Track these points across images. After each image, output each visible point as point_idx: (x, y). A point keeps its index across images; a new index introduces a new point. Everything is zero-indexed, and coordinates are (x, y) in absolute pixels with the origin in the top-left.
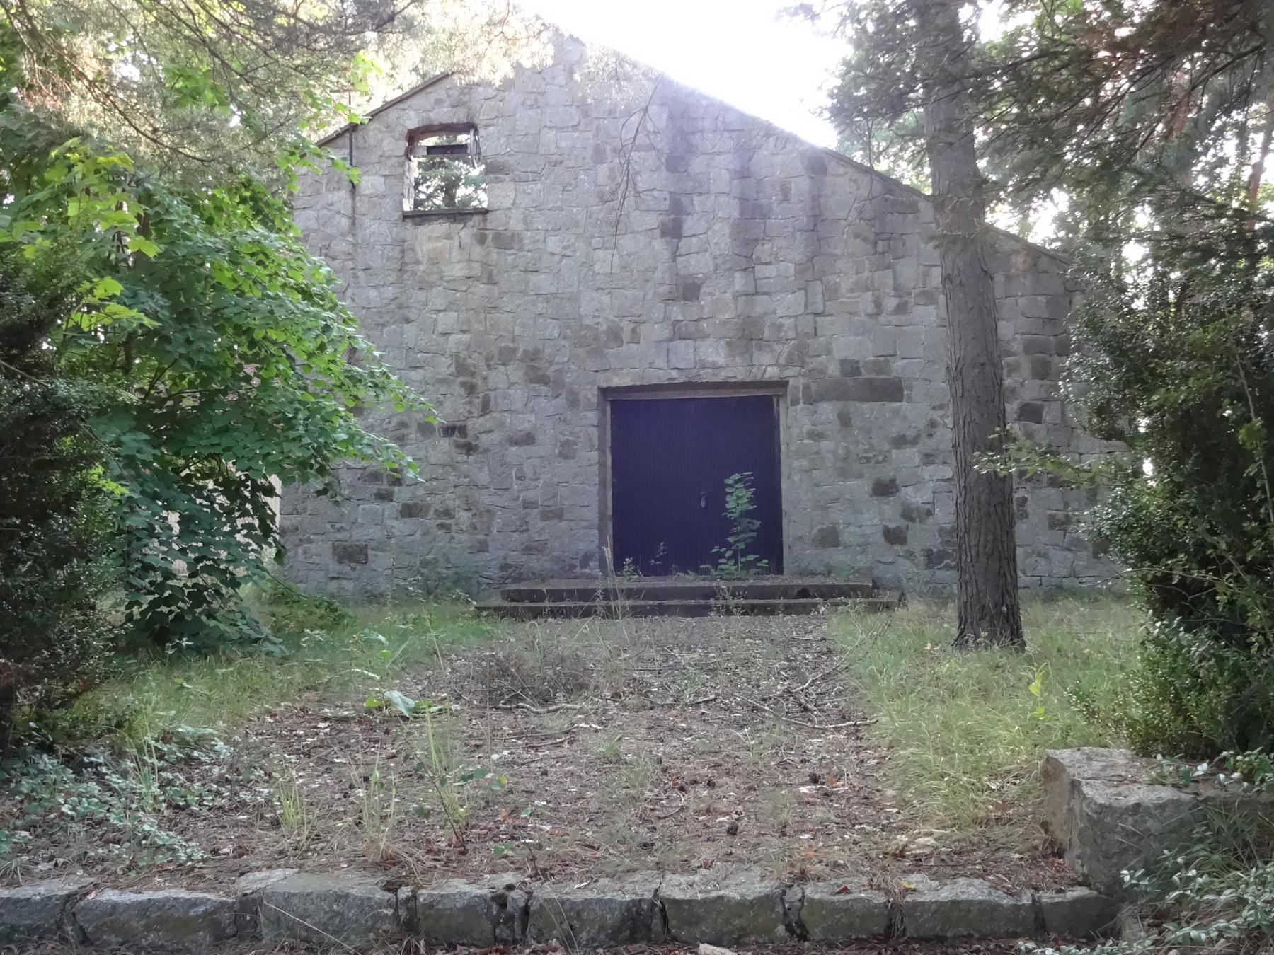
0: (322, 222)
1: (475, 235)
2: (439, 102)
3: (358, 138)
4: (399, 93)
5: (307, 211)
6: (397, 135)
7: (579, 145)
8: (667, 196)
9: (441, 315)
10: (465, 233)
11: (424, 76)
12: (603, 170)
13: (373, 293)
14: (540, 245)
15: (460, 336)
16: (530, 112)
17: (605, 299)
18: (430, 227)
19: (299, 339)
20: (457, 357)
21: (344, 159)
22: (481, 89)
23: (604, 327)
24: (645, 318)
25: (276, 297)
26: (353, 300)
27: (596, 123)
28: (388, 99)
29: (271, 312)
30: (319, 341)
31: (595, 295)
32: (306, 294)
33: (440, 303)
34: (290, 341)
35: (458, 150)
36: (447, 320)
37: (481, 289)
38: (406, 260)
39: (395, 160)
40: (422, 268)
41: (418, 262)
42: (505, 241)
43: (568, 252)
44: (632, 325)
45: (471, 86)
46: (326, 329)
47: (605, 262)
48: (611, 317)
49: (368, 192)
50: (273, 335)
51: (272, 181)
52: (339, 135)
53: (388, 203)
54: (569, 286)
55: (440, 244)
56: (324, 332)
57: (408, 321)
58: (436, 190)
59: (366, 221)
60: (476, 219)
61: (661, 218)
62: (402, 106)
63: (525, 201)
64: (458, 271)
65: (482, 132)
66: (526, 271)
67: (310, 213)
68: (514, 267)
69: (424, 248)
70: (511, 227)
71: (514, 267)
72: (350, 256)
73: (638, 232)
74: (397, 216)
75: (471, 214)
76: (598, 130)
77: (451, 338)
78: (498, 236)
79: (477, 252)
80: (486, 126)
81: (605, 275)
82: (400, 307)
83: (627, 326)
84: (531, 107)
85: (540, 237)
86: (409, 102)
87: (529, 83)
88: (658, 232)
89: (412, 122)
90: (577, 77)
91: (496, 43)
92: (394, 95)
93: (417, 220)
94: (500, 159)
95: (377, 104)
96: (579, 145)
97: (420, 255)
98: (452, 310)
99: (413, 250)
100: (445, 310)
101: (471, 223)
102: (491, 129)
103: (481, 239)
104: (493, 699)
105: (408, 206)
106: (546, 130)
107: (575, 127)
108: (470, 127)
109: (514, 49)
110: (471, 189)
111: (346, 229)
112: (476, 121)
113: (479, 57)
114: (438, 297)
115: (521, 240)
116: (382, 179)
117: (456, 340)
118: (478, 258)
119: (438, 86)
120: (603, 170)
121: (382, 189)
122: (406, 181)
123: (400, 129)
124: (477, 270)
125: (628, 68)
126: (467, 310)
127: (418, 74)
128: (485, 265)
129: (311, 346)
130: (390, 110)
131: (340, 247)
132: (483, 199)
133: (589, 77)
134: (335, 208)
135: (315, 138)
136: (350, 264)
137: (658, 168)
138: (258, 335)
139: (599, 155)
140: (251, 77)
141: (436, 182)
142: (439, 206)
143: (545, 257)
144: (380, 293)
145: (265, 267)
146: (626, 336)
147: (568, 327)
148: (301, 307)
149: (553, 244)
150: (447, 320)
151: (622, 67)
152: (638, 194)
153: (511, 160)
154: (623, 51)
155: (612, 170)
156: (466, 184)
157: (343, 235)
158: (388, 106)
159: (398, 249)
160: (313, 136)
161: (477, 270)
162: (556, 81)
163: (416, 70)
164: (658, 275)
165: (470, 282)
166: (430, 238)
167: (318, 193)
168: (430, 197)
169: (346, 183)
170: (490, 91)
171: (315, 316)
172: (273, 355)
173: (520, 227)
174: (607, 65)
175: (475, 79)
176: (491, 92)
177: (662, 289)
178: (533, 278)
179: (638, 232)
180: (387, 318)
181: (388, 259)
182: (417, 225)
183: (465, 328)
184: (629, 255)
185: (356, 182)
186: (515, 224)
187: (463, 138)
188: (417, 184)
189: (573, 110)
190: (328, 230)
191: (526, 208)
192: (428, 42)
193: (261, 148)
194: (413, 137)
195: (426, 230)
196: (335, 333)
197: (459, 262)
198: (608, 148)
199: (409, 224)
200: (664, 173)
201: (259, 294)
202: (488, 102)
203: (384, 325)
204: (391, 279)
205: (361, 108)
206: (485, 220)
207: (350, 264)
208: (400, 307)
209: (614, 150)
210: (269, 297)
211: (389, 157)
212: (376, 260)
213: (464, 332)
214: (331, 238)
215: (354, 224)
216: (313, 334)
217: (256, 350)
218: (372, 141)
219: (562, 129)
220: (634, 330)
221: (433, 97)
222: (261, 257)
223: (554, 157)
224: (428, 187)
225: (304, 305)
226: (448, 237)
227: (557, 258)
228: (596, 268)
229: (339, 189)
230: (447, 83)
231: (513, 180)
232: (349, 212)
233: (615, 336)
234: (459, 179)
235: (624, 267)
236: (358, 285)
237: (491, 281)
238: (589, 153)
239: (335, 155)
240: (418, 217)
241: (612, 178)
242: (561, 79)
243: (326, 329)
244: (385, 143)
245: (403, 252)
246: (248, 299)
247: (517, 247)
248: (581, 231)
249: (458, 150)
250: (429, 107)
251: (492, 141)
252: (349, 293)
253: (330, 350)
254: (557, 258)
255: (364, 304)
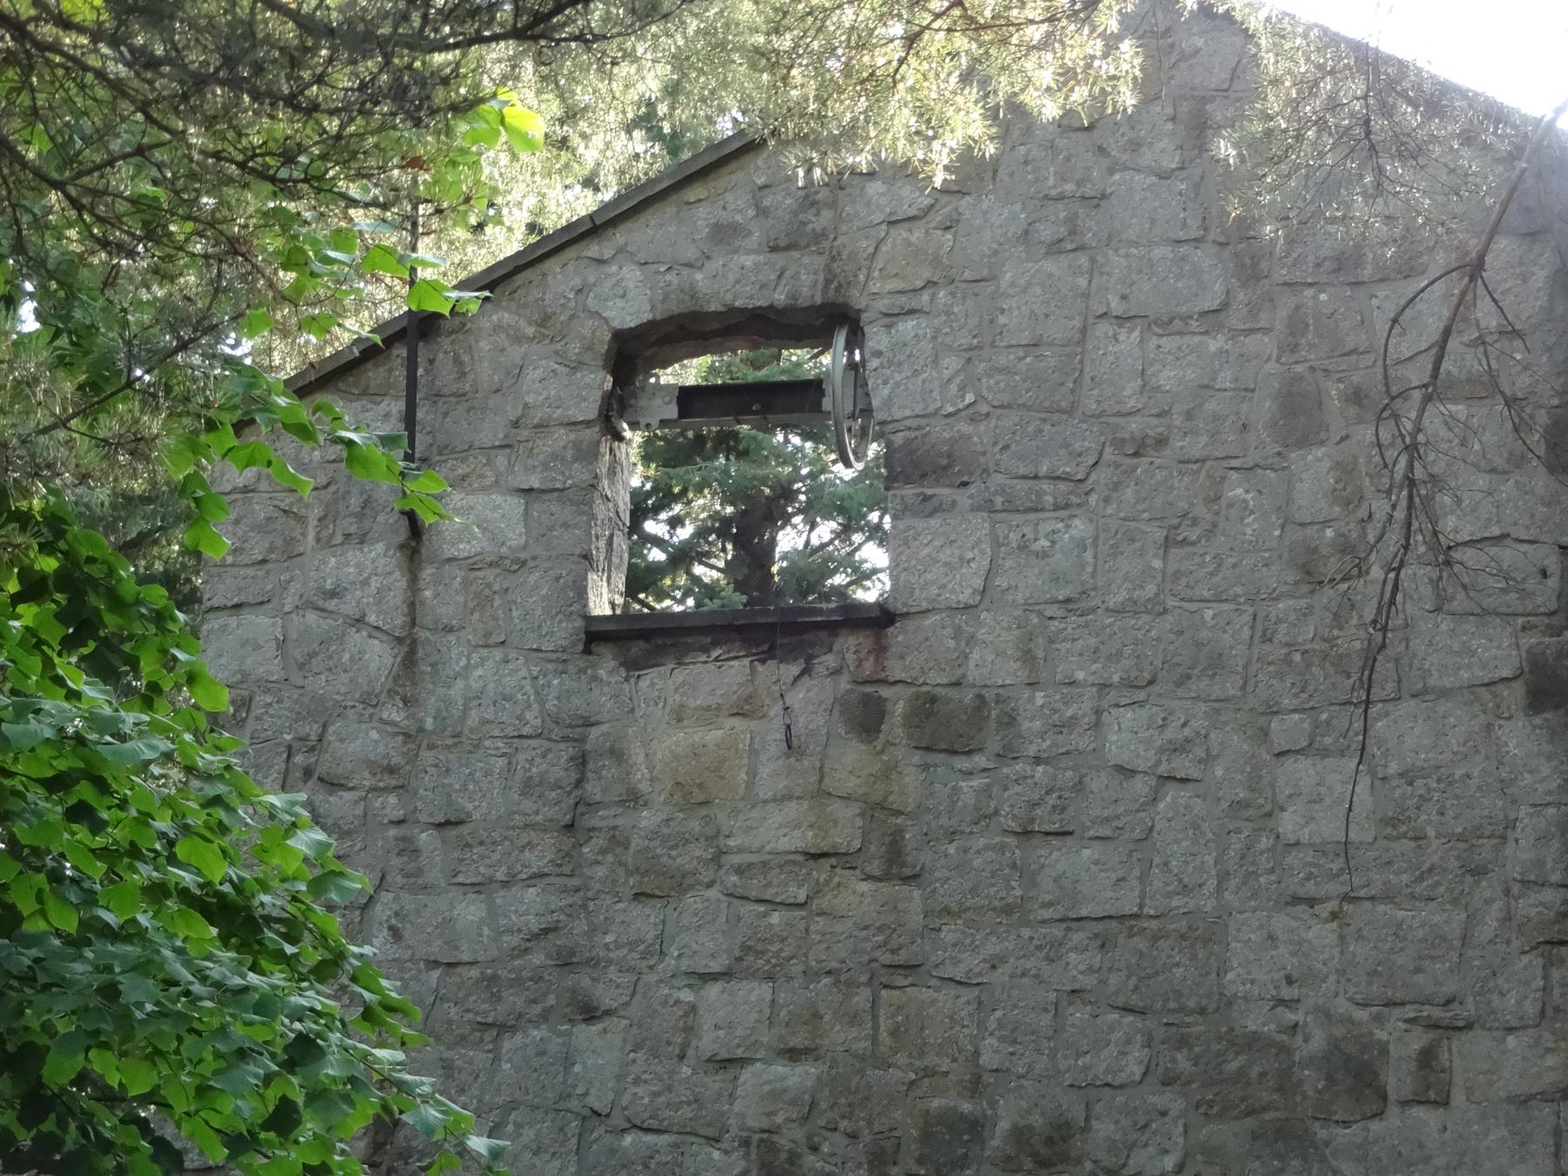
0: (298, 654)
1: (841, 702)
2: (724, 234)
3: (439, 362)
4: (584, 204)
5: (248, 617)
6: (575, 348)
7: (1225, 378)
8: (1553, 562)
9: (713, 991)
10: (810, 695)
11: (673, 144)
12: (1314, 470)
13: (470, 911)
14: (1084, 742)
15: (780, 1069)
16: (1050, 266)
17: (1321, 935)
18: (681, 675)
19: (203, 1091)
20: (769, 1147)
21: (388, 441)
22: (874, 188)
23: (1318, 1042)
24: (1470, 1008)
25: (129, 933)
26: (396, 934)
27: (1286, 305)
28: (551, 223)
29: (110, 992)
30: (273, 1095)
31: (1281, 922)
32: (232, 916)
33: (710, 949)
34: (168, 1093)
35: (798, 400)
36: (734, 1011)
37: (858, 896)
38: (593, 790)
39: (562, 437)
40: (647, 819)
41: (633, 799)
42: (950, 726)
43: (1183, 765)
44: (1418, 1040)
45: (840, 182)
46: (303, 1051)
47: (1320, 800)
48: (1342, 1006)
49: (464, 549)
50: (108, 1068)
51: (128, 502)
52: (368, 353)
53: (535, 590)
54: (1185, 889)
55: (714, 736)
56: (290, 1065)
57: (590, 1013)
58: (702, 533)
59: (456, 653)
60: (851, 644)
61: (1530, 640)
62: (593, 249)
63: (1025, 582)
64: (778, 830)
65: (876, 337)
66: (1026, 834)
67: (261, 624)
68: (984, 817)
69: (661, 752)
70: (973, 674)
71: (984, 817)
72: (393, 776)
73: (1444, 694)
74: (565, 632)
75: (832, 628)
76: (1297, 326)
77: (747, 1075)
78: (926, 708)
79: (851, 762)
80: (892, 317)
81: (1320, 850)
82: (566, 962)
83: (1401, 1041)
84: (1054, 248)
85: (1083, 708)
86: (620, 236)
87: (1050, 175)
88: (1515, 694)
89: (627, 296)
90: (1225, 149)
91: (935, 42)
92: (571, 204)
93: (637, 648)
94: (941, 432)
95: (506, 242)
96: (1225, 378)
97: (641, 775)
98: (751, 975)
99: (617, 755)
100: (726, 975)
101: (830, 660)
102: (908, 326)
103: (866, 718)
104: (1164, 1084)
105: (603, 599)
106: (1104, 328)
107: (1213, 318)
108: (831, 320)
109: (999, 56)
110: (825, 530)
111: (381, 681)
112: (858, 299)
113: (878, 85)
114: (703, 928)
115: (1009, 721)
116: (515, 505)
117: (769, 1083)
118: (851, 784)
119: (723, 180)
120: (1314, 470)
121: (515, 536)
122: (601, 510)
123: (586, 327)
124: (846, 829)
125: (1410, 117)
126: (810, 975)
127: (655, 134)
128: (877, 809)
129: (243, 1106)
130: (553, 264)
131: (359, 743)
132: (874, 571)
133: (1264, 150)
134: (348, 606)
135: (285, 362)
136: (392, 806)
137: (1517, 461)
138: (58, 1071)
139: (1298, 418)
140: (97, 193)
141: (706, 504)
142: (711, 591)
143: (1097, 783)
144: (493, 913)
145: (97, 826)
146: (1397, 1079)
147: (1183, 1042)
148: (215, 972)
149: (1128, 735)
150: (734, 1011)
151: (1387, 111)
152: (1444, 555)
153: (979, 435)
154: (1392, 42)
155: (1345, 469)
156: (812, 513)
157: (370, 701)
158: (549, 247)
159: (565, 752)
160: (270, 351)
161: (846, 829)
162: (1147, 157)
163: (646, 121)
164: (1520, 854)
165: (821, 872)
166: (679, 716)
167: (291, 554)
168: (682, 557)
169: (388, 521)
170: (907, 191)
171: (266, 1007)
172: (106, 1146)
173: (1009, 673)
174: (1333, 105)
175: (863, 161)
176: (909, 199)
177: (1530, 906)
178: (1057, 860)
179: (1444, 694)
180: (514, 1000)
181: (528, 786)
182: (633, 666)
183: (798, 1041)
184: (1408, 776)
185: (428, 519)
186: (991, 662)
187: (799, 360)
188: (641, 510)
189: (1204, 257)
190: (319, 684)
191: (1028, 607)
192: (693, 25)
193: (108, 426)
194: (630, 355)
195: (663, 683)
196: (331, 1070)
197: (787, 797)
198: (1334, 391)
199: (607, 665)
200: (1541, 481)
201: (70, 925)
202: (901, 233)
203: (504, 1028)
204: (536, 860)
205: (448, 261)
206: (880, 650)
207: (392, 806)
208: (566, 962)
209: (1356, 397)
210: (106, 932)
211: (542, 426)
212: (485, 793)
213: (793, 1055)
214: (324, 713)
215: (410, 661)
216: (253, 1072)
217: (49, 1125)
218: (485, 372)
219: (1167, 324)
220: (1427, 1058)
221: (704, 216)
222: (84, 791)
223: (1134, 426)
224: (675, 522)
225: (224, 964)
226: (745, 709)
227: (1141, 786)
228: (1289, 823)
229: (363, 539)
230: (756, 170)
231: (987, 506)
232: (399, 620)
233: (1358, 1079)
234: (787, 494)
235: (1391, 823)
236: (416, 882)
237: (897, 866)
238: (1262, 409)
239: (362, 424)
240: (637, 640)
241: (1348, 498)
242: (1164, 151)
243: (303, 1051)
244: (533, 375)
245: (581, 761)
246: (34, 940)
247: (994, 744)
248: (1231, 689)
249: (798, 400)
250: (691, 253)
251: (909, 368)
252: (381, 912)
253: (310, 1126)
254: (1141, 786)
255: (436, 949)
